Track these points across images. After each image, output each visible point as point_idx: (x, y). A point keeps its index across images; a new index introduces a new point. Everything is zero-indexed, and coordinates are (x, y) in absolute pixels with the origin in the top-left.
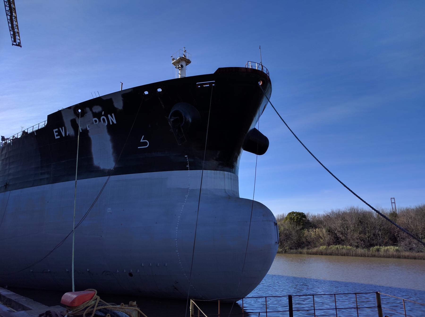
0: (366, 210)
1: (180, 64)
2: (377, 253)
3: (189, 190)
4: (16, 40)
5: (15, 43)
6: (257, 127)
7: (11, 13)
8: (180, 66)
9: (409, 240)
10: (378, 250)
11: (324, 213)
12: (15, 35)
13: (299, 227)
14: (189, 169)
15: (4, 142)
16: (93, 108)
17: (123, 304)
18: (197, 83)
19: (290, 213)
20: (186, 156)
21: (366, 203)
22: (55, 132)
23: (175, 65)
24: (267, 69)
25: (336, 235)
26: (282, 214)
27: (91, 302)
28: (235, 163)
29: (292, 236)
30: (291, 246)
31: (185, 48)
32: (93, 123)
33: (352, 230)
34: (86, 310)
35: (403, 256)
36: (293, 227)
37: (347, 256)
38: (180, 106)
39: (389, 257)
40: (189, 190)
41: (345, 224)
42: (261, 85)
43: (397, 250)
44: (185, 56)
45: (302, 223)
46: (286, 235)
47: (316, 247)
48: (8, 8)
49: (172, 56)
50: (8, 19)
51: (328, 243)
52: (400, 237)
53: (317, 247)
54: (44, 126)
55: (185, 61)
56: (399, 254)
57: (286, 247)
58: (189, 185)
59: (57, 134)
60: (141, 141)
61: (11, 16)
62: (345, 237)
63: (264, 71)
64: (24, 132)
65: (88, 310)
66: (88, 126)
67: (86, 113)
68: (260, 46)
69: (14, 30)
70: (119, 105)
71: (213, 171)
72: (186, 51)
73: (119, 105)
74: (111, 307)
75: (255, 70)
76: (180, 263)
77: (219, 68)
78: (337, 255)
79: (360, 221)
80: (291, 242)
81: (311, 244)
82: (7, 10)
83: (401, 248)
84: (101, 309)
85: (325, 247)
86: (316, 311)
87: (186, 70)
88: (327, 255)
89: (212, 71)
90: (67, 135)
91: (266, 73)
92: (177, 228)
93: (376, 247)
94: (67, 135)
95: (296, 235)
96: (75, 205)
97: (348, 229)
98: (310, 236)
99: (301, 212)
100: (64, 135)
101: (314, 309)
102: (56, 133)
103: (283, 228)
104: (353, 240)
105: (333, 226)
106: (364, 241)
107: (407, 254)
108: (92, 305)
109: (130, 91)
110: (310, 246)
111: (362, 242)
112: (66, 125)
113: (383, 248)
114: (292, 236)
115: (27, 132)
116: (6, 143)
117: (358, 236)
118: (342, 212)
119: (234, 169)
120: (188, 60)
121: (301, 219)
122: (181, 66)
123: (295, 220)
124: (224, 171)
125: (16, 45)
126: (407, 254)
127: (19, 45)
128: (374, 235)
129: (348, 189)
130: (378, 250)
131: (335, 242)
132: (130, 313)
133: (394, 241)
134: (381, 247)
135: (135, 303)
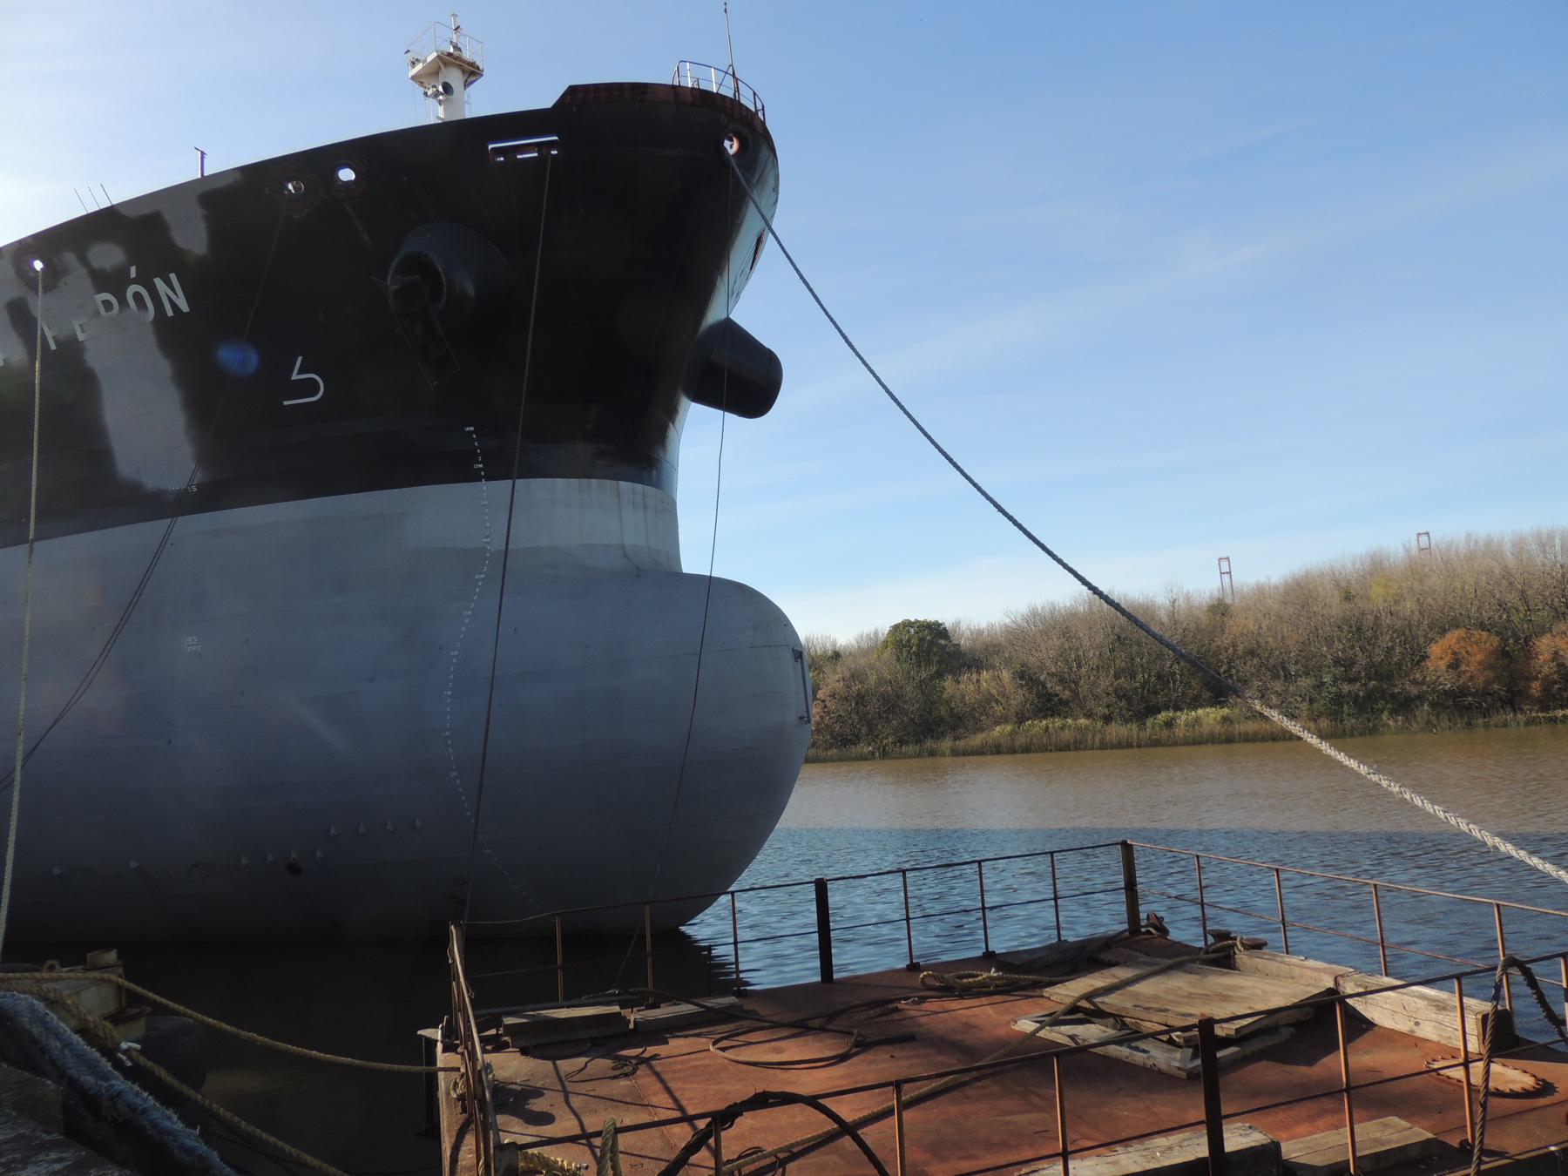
0: (1137, 597)
1: (442, 78)
2: (1165, 733)
3: (488, 555)
6: (738, 317)
8: (441, 89)
9: (1260, 683)
10: (1169, 724)
11: (1007, 621)
13: (925, 670)
14: (484, 477)
18: (490, 147)
19: (896, 628)
23: (421, 83)
24: (755, 94)
25: (1044, 687)
31: (454, 15)
32: (98, 313)
33: (1092, 669)
35: (1240, 734)
36: (908, 673)
38: (428, 236)
39: (1199, 741)
41: (1070, 648)
42: (737, 154)
43: (1225, 719)
44: (456, 48)
46: (885, 699)
47: (982, 730)
49: (409, 51)
51: (1017, 713)
52: (1235, 677)
55: (460, 67)
56: (1231, 729)
58: (487, 537)
60: (295, 377)
63: (743, 101)
66: (81, 325)
67: (66, 272)
68: (725, 4)
71: (574, 481)
72: (458, 27)
73: (192, 237)
75: (712, 93)
77: (570, 87)
79: (1119, 637)
80: (902, 721)
81: (967, 722)
83: (1237, 711)
85: (1009, 728)
87: (466, 106)
88: (1014, 752)
89: (544, 97)
91: (754, 110)
92: (450, 693)
93: (1163, 716)
95: (917, 695)
97: (1079, 666)
98: (963, 697)
103: (875, 677)
104: (1096, 697)
106: (1128, 699)
109: (229, 181)
111: (1124, 702)
113: (1183, 717)
117: (1112, 685)
118: (1062, 611)
119: (654, 472)
120: (472, 66)
121: (932, 643)
122: (443, 88)
123: (914, 649)
124: (616, 478)
128: (1159, 677)
129: (1010, 518)
130: (1169, 724)
133: (1219, 692)
134: (1179, 714)
135: (111, 956)
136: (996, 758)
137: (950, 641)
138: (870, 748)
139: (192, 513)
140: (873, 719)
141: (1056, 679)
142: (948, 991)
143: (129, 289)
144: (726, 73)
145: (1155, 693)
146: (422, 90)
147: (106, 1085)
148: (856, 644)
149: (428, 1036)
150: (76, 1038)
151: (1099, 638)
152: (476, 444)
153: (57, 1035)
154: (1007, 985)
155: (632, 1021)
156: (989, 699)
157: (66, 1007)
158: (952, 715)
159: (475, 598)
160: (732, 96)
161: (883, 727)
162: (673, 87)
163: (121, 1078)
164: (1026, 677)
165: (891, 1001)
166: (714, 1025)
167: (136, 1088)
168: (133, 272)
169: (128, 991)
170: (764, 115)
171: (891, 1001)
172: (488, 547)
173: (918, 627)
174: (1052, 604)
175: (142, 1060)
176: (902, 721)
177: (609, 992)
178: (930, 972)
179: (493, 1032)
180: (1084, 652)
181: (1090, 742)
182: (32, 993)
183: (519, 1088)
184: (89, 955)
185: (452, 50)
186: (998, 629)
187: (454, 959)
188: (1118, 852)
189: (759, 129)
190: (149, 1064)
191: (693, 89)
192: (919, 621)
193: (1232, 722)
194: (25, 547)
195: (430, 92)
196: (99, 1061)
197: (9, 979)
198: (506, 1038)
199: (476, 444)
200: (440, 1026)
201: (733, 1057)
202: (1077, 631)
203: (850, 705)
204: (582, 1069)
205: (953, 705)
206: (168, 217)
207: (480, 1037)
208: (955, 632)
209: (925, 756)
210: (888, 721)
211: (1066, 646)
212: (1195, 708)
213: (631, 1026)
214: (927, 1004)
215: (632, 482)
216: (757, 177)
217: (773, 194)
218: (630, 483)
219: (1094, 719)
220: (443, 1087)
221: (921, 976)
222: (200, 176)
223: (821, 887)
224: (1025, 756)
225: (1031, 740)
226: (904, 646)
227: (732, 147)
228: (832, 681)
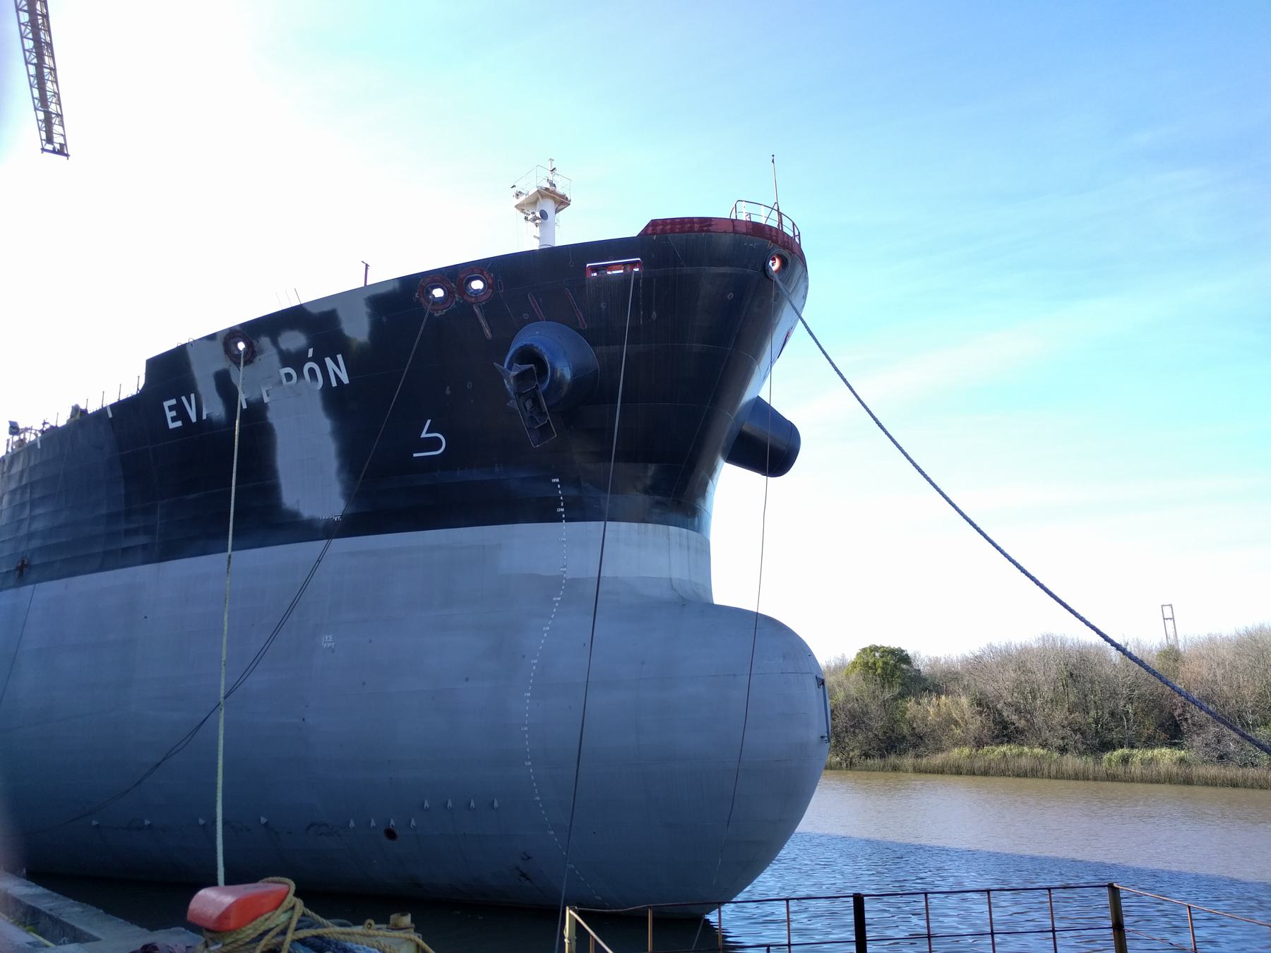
2: (1120, 770)
3: (564, 581)
4: (54, 135)
5: (49, 147)
6: (764, 395)
7: (40, 56)
8: (538, 214)
10: (1125, 760)
15: (16, 438)
17: (372, 922)
18: (588, 265)
20: (554, 480)
22: (167, 410)
23: (522, 211)
24: (794, 224)
25: (1000, 714)
28: (700, 501)
34: (263, 942)
40: (564, 581)
43: (1182, 760)
46: (852, 715)
52: (1190, 721)
54: (134, 393)
55: (553, 198)
57: (853, 750)
58: (565, 567)
59: (174, 413)
60: (424, 435)
61: (40, 66)
63: (785, 230)
64: (76, 409)
66: (267, 391)
67: (261, 352)
68: (773, 156)
70: (358, 329)
71: (635, 525)
73: (358, 329)
76: (538, 798)
79: (1071, 674)
81: (927, 741)
83: (1192, 754)
85: (966, 751)
87: (556, 227)
88: (974, 774)
89: (632, 229)
90: (204, 417)
92: (529, 694)
93: (1119, 752)
100: (194, 419)
104: (1051, 729)
105: (990, 689)
107: (1213, 771)
108: (277, 930)
111: (1079, 736)
112: (201, 388)
113: (1139, 754)
114: (870, 719)
116: (22, 441)
119: (696, 518)
120: (562, 198)
121: (895, 666)
123: (879, 671)
124: (668, 523)
125: (54, 151)
126: (1213, 771)
127: (62, 151)
128: (1112, 714)
130: (1125, 760)
131: (997, 737)
133: (1173, 732)
134: (1135, 751)
135: (407, 920)
136: (956, 778)
138: (838, 759)
141: (1014, 708)
143: (307, 364)
144: (772, 209)
145: (1110, 730)
146: (524, 215)
151: (1053, 674)
158: (914, 734)
159: (553, 616)
161: (850, 740)
162: (733, 221)
164: (981, 703)
168: (310, 354)
173: (883, 652)
181: (1046, 771)
188: (1105, 891)
189: (796, 250)
192: (884, 647)
193: (1190, 765)
205: (915, 725)
208: (915, 657)
209: (888, 770)
212: (1152, 748)
215: (679, 527)
219: (1049, 750)
222: (363, 286)
223: (859, 900)
224: (984, 778)
226: (871, 668)
227: (775, 265)
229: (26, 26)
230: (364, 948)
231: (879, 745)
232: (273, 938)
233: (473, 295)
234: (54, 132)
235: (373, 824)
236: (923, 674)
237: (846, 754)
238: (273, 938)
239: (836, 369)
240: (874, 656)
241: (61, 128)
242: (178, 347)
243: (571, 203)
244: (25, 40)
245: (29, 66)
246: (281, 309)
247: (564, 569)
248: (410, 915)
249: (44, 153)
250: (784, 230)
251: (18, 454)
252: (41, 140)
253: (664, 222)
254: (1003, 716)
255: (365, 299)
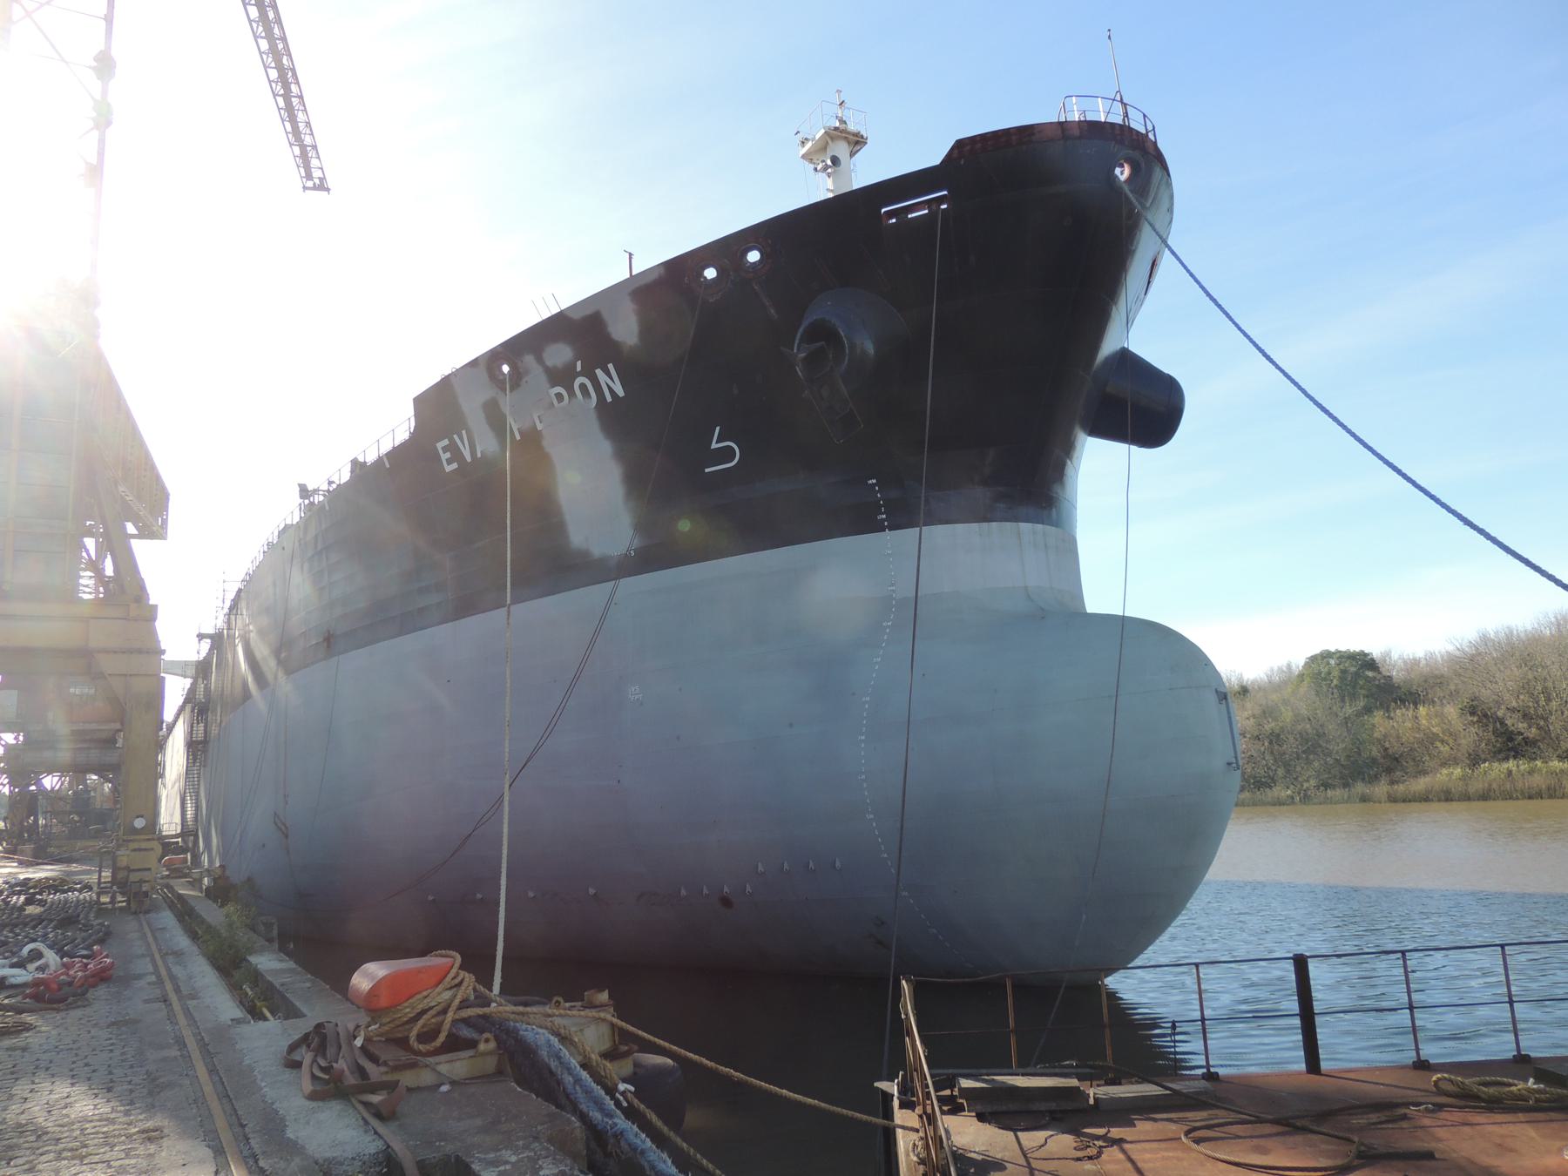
1: (830, 153)
3: (894, 603)
4: (313, 170)
5: (310, 184)
7: (286, 86)
8: (829, 162)
11: (1451, 648)
12: (305, 155)
13: (1350, 705)
15: (307, 502)
16: (545, 355)
17: (560, 999)
18: (883, 211)
19: (1313, 659)
20: (870, 482)
21: (1558, 580)
22: (441, 452)
24: (1145, 116)
26: (1285, 664)
27: (439, 994)
28: (1056, 488)
29: (1328, 742)
30: (1326, 776)
34: (421, 1022)
37: (1549, 798)
40: (894, 603)
42: (1128, 180)
45: (1363, 692)
46: (1303, 738)
47: (1425, 773)
48: (274, 74)
49: (798, 132)
50: (279, 109)
51: (1470, 755)
53: (1428, 773)
57: (1308, 781)
58: (893, 585)
59: (448, 455)
60: (714, 446)
61: (287, 97)
62: (1539, 728)
63: (1133, 125)
64: (355, 462)
65: (429, 1020)
66: (539, 417)
68: (1109, 30)
69: (303, 141)
70: (625, 329)
71: (975, 526)
72: (843, 102)
73: (625, 329)
74: (506, 1012)
75: (1100, 122)
76: (885, 856)
78: (1508, 796)
80: (1326, 763)
81: (1405, 763)
82: (271, 79)
84: (470, 1017)
85: (1458, 771)
86: (1296, 1010)
88: (1469, 799)
89: (933, 156)
90: (479, 455)
91: (1144, 132)
92: (863, 738)
94: (479, 455)
96: (508, 685)
97: (1548, 700)
99: (1357, 650)
100: (469, 459)
101: (1512, 1006)
102: (444, 453)
103: (1290, 714)
105: (1486, 694)
108: (439, 1008)
109: (654, 276)
110: (1400, 771)
114: (1328, 742)
115: (365, 462)
116: (312, 504)
118: (1522, 635)
119: (1054, 510)
121: (1357, 674)
123: (1335, 682)
124: (1016, 519)
125: (315, 188)
127: (322, 186)
129: (1481, 531)
131: (1500, 751)
132: (567, 1031)
135: (604, 997)
137: (1380, 673)
138: (1289, 792)
139: (630, 576)
140: (1291, 760)
142: (1468, 1099)
146: (812, 166)
147: (610, 1122)
148: (1266, 678)
149: (884, 1088)
150: (584, 1075)
152: (879, 495)
153: (569, 1070)
154: (1554, 1101)
155: (1092, 1095)
156: (1432, 739)
157: (572, 1043)
160: (1121, 122)
161: (1302, 768)
162: (1060, 123)
163: (623, 1117)
164: (1477, 711)
165: (1398, 1105)
166: (1189, 1110)
167: (635, 1128)
168: (579, 368)
169: (621, 1030)
170: (1155, 136)
171: (1398, 1105)
172: (894, 595)
174: (1508, 628)
175: (636, 1102)
176: (1326, 763)
177: (1066, 1063)
178: (1445, 1075)
179: (947, 1092)
180: (1553, 683)
182: (546, 1028)
183: (979, 1158)
184: (586, 993)
185: (837, 124)
186: (1439, 659)
187: (907, 1014)
189: (1151, 150)
190: (642, 1107)
191: (1080, 122)
192: (1340, 652)
194: (503, 611)
195: (819, 167)
196: (604, 1099)
197: (527, 1013)
198: (961, 1101)
199: (879, 495)
200: (896, 1081)
201: (1209, 1153)
202: (1542, 659)
203: (1263, 745)
204: (1043, 1146)
205: (1387, 745)
206: (606, 315)
207: (937, 1096)
210: (1309, 762)
211: (1530, 676)
213: (1091, 1101)
214: (1444, 1114)
216: (1150, 201)
217: (1168, 214)
218: (1030, 524)
220: (902, 1147)
221: (1434, 1078)
222: (628, 276)
223: (1300, 963)
224: (1481, 804)
225: (1490, 785)
226: (1324, 679)
227: (1123, 173)
228: (1243, 716)
229: (268, 54)
230: (533, 1029)
231: (1341, 773)
232: (433, 1017)
233: (751, 270)
234: (312, 166)
235: (705, 891)
236: (1394, 680)
237: (1299, 786)
238: (433, 1017)
239: (1208, 295)
240: (1328, 663)
241: (317, 160)
242: (442, 379)
243: (868, 141)
244: (268, 70)
245: (277, 98)
246: (540, 320)
247: (894, 588)
248: (607, 991)
249: (307, 191)
250: (1132, 126)
251: (310, 516)
252: (301, 177)
253: (972, 140)
254: (1506, 725)
255: (630, 294)
